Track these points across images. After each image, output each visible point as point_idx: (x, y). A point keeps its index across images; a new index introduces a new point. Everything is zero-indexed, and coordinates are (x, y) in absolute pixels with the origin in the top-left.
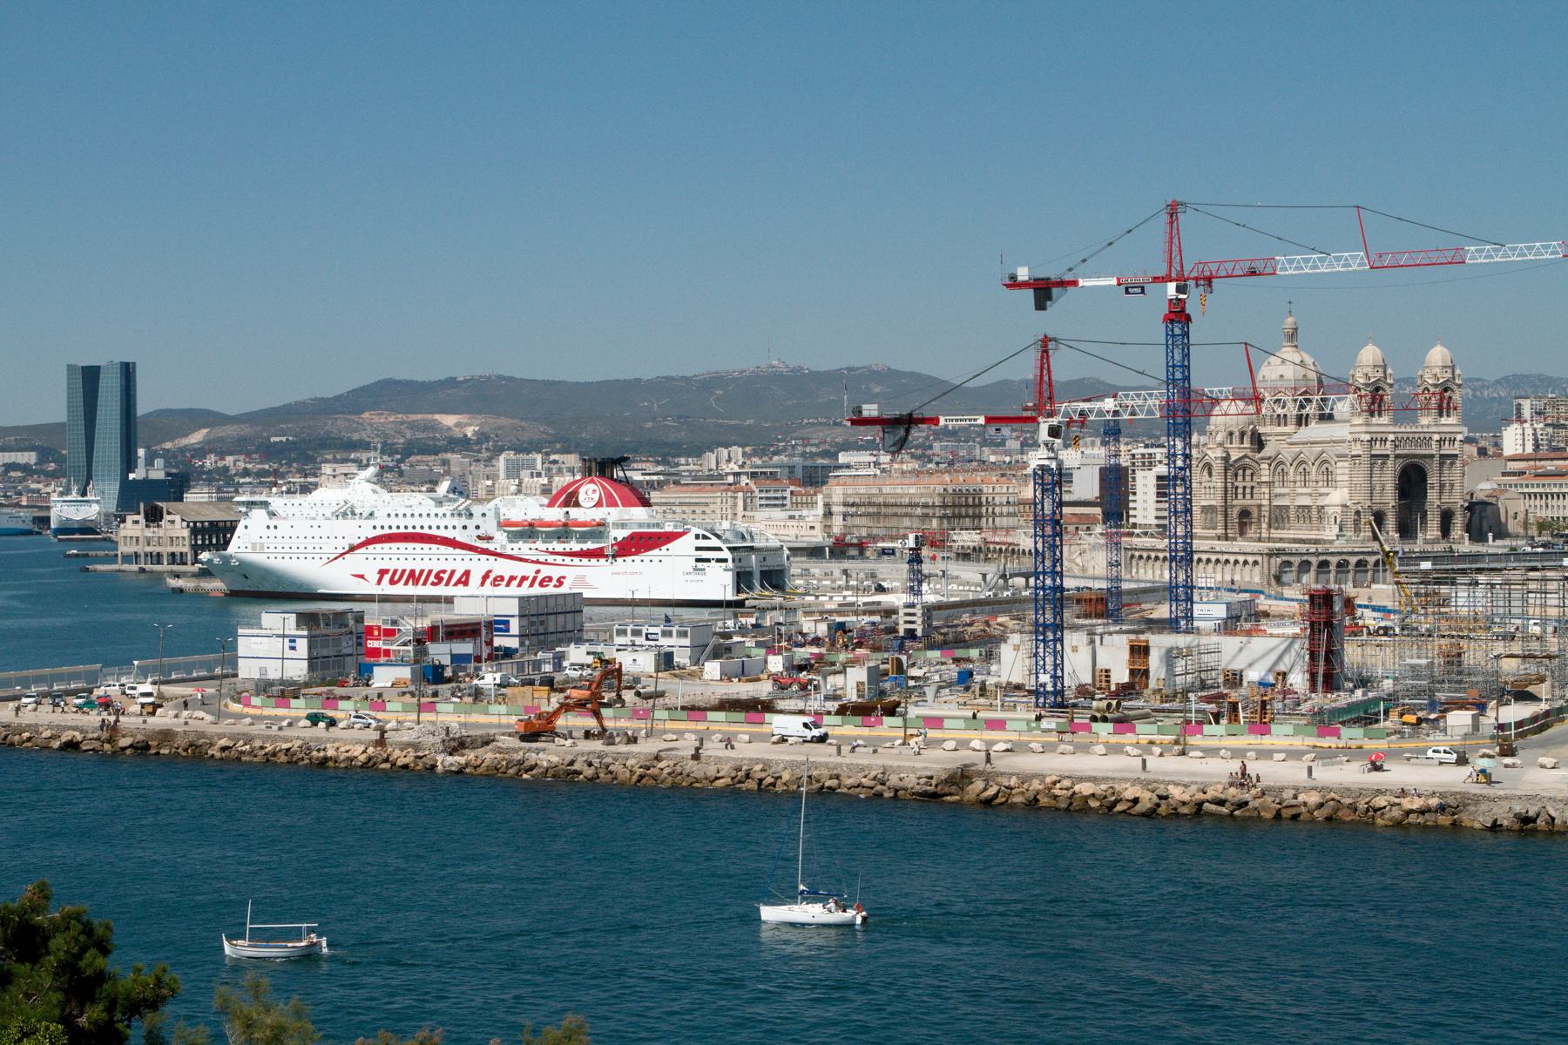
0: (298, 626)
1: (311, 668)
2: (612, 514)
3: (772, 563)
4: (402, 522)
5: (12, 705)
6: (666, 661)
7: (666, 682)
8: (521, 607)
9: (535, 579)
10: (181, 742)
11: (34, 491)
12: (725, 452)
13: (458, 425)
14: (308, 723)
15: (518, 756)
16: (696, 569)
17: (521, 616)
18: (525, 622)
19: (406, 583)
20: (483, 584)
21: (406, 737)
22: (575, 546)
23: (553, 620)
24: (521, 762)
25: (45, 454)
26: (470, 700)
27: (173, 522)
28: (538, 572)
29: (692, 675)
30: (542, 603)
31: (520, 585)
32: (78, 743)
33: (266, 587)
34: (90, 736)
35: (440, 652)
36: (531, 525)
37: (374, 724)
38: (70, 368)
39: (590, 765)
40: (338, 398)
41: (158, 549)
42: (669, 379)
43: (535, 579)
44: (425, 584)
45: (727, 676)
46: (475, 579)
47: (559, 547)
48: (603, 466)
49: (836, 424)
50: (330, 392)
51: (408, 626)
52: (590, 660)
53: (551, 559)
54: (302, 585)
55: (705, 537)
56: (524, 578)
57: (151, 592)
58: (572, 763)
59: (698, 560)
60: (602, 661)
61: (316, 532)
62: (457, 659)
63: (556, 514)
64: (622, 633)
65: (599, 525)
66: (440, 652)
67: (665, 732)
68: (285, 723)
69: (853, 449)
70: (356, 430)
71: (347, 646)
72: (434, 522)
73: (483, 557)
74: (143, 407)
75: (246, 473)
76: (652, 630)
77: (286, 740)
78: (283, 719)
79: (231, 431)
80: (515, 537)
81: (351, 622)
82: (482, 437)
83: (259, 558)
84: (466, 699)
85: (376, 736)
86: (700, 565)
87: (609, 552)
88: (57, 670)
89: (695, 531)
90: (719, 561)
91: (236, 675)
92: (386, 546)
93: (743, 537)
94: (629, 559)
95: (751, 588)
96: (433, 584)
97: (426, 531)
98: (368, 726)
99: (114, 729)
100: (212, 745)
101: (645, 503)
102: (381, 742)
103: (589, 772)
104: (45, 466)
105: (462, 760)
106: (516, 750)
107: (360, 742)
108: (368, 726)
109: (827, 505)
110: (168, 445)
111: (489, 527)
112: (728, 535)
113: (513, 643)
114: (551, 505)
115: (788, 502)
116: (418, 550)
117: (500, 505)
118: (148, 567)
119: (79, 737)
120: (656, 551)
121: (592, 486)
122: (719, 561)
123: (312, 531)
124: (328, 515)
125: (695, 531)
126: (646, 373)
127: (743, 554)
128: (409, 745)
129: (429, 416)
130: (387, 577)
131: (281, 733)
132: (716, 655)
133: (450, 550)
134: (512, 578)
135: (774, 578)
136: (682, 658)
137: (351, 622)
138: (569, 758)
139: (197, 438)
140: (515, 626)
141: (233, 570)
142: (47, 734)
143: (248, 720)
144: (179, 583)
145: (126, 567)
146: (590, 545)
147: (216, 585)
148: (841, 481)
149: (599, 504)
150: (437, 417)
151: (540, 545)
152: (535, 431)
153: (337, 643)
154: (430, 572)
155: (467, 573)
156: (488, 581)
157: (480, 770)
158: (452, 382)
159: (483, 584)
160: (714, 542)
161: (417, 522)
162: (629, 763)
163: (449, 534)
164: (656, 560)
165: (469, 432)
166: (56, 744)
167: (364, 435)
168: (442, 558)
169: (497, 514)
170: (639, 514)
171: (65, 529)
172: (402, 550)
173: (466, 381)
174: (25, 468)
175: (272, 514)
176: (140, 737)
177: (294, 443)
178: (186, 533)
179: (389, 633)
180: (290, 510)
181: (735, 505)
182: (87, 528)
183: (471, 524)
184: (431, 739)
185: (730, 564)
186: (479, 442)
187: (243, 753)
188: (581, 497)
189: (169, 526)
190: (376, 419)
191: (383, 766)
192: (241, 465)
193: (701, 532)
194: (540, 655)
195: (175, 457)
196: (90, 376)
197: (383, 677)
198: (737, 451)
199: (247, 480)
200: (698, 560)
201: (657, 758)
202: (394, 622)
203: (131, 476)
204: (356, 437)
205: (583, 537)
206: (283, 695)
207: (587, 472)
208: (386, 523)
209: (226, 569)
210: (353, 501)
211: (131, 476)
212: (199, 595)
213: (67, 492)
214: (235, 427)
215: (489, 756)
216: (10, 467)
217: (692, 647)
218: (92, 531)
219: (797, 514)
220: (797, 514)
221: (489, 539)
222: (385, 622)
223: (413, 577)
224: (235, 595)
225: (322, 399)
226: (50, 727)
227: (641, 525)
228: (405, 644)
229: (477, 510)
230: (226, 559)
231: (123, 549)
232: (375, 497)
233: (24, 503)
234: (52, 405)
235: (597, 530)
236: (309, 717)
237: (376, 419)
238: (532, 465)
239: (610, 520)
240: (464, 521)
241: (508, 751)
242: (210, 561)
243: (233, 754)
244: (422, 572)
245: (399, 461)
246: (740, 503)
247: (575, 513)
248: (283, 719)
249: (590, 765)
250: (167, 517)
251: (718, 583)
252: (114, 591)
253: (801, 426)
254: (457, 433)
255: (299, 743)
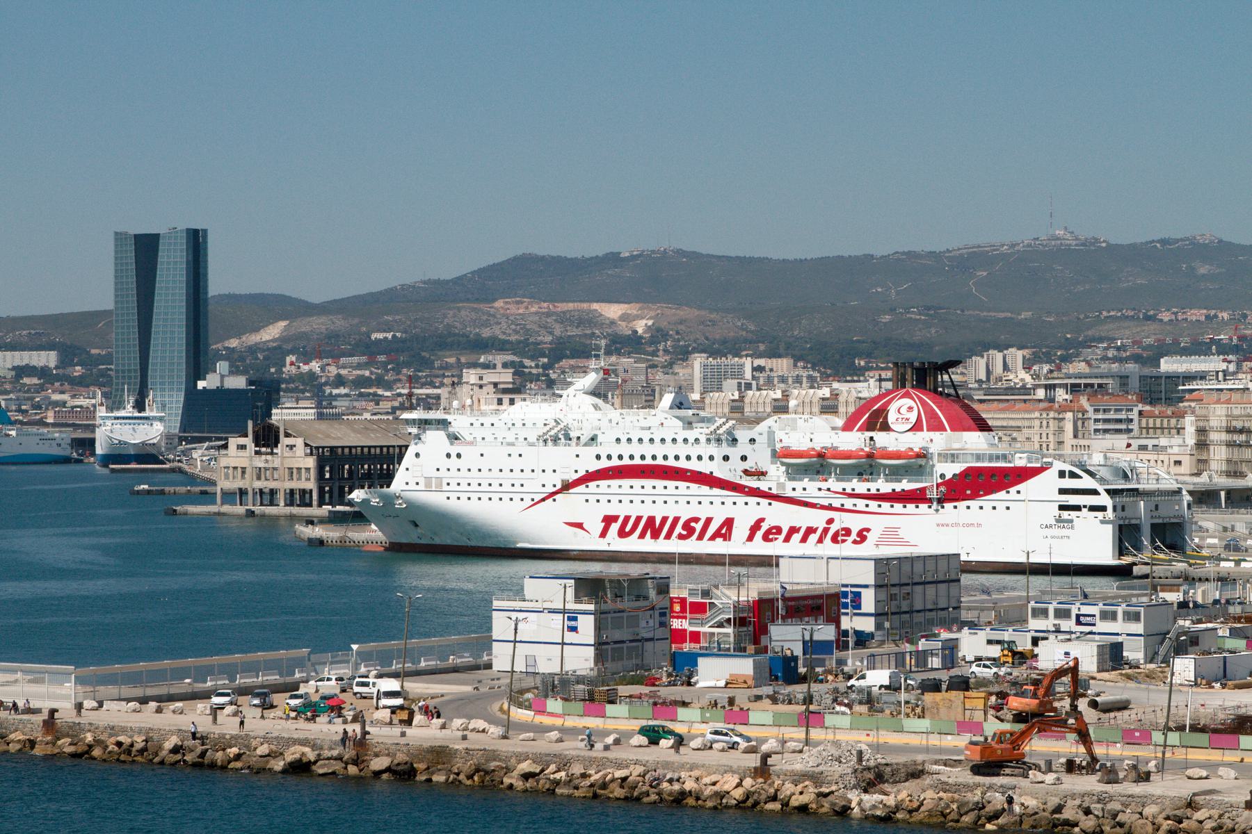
0: (578, 599)
1: (600, 657)
2: (937, 442)
3: (1166, 513)
4: (637, 450)
5: (201, 706)
6: (1113, 656)
7: (1110, 687)
8: (877, 574)
9: (826, 530)
10: (463, 765)
11: (56, 404)
12: (999, 356)
13: (624, 317)
14: (643, 740)
15: (975, 797)
16: (1059, 520)
17: (878, 586)
18: (883, 596)
19: (642, 536)
20: (750, 538)
21: (799, 764)
22: (885, 487)
23: (920, 596)
24: (980, 807)
25: (68, 355)
26: (864, 709)
27: (291, 447)
28: (830, 521)
29: (1150, 676)
30: (906, 568)
31: (804, 540)
32: (309, 763)
33: (464, 542)
34: (327, 753)
35: (787, 637)
36: (821, 455)
37: (743, 745)
38: (119, 237)
39: (1087, 812)
40: (458, 281)
41: (272, 485)
42: (910, 255)
43: (826, 530)
44: (668, 537)
45: (1203, 679)
46: (741, 530)
47: (861, 487)
48: (924, 375)
49: (1148, 318)
50: (448, 272)
51: (727, 598)
52: (995, 651)
53: (849, 503)
54: (497, 536)
55: (1073, 475)
56: (810, 531)
57: (266, 542)
58: (1059, 809)
59: (1062, 508)
60: (1014, 654)
61: (516, 463)
62: (811, 646)
63: (854, 441)
64: (1041, 613)
65: (918, 456)
66: (787, 637)
67: (1187, 765)
68: (610, 740)
69: (1176, 353)
70: (486, 324)
71: (647, 626)
72: (682, 450)
73: (753, 500)
74: (218, 284)
75: (340, 381)
76: (1086, 610)
77: (620, 765)
78: (606, 733)
79: (317, 325)
80: (796, 472)
81: (652, 593)
82: (658, 335)
83: (435, 499)
84: (857, 708)
85: (753, 761)
86: (1065, 515)
87: (934, 495)
88: (251, 657)
89: (1059, 465)
90: (1093, 508)
91: (489, 666)
92: (615, 483)
93: (1125, 476)
94: (962, 505)
95: (1138, 548)
96: (681, 537)
97: (671, 462)
98: (734, 746)
99: (362, 743)
100: (508, 770)
101: (983, 426)
102: (763, 771)
103: (1089, 823)
104: (69, 370)
105: (891, 801)
106: (971, 788)
107: (730, 770)
108: (734, 746)
109: (1201, 431)
110: (233, 343)
111: (760, 458)
112: (1103, 472)
113: (867, 625)
114: (848, 427)
115: (1134, 426)
116: (671, 490)
117: (775, 427)
118: (258, 509)
119: (311, 755)
120: (1001, 495)
121: (907, 402)
122: (1093, 508)
123: (492, 456)
124: (532, 439)
125: (1059, 465)
126: (881, 248)
127: (1125, 499)
128: (805, 776)
129: (585, 306)
130: (615, 527)
131: (610, 755)
132: (1180, 650)
133: (705, 489)
134: (793, 530)
135: (1170, 535)
136: (1134, 652)
137: (652, 593)
138: (1054, 802)
139: (271, 333)
140: (868, 601)
141: (397, 514)
142: (263, 750)
143: (554, 735)
144: (318, 532)
145: (226, 508)
146: (905, 485)
147: (372, 534)
148: (1224, 396)
149: (917, 427)
150: (595, 306)
151: (834, 484)
152: (730, 326)
153: (634, 621)
154: (676, 520)
155: (729, 523)
156: (759, 534)
157: (918, 817)
158: (613, 259)
159: (750, 538)
160: (1086, 482)
161: (659, 450)
162: (1150, 810)
163: (704, 467)
164: (1001, 506)
165: (640, 326)
166: (278, 765)
167: (497, 331)
168: (694, 500)
169: (771, 434)
170: (974, 441)
171: (117, 456)
172: (637, 489)
173: (633, 258)
174: (43, 372)
175: (454, 438)
176: (401, 757)
177: (403, 341)
178: (311, 462)
179: (699, 608)
180: (478, 433)
181: (1061, 430)
182: (146, 455)
183: (735, 453)
184: (837, 769)
185: (1110, 514)
186: (654, 341)
187: (557, 783)
188: (892, 417)
189: (287, 453)
190: (513, 309)
191: (770, 806)
192: (333, 370)
193: (1067, 468)
194: (923, 644)
195: (242, 359)
196: (145, 249)
197: (713, 673)
198: (1017, 356)
199: (343, 391)
200: (1062, 508)
201: (1191, 805)
202: (706, 593)
203: (201, 385)
204: (486, 333)
205: (895, 473)
206: (591, 698)
207: (900, 382)
208: (613, 452)
209: (388, 512)
210: (567, 420)
211: (201, 385)
212: (346, 548)
213: (119, 405)
214: (323, 319)
215: (930, 794)
216: (21, 371)
217: (1147, 635)
218: (152, 458)
219: (1150, 443)
220: (1150, 443)
221: (761, 474)
222: (692, 592)
223: (653, 528)
224: (396, 548)
225: (438, 283)
226: (266, 739)
227: (979, 457)
228: (720, 625)
229: (743, 435)
230: (389, 500)
231: (225, 484)
232: (598, 414)
233: (50, 420)
234: (95, 287)
235: (917, 463)
236: (644, 731)
237: (513, 309)
238: (738, 373)
239: (934, 449)
240: (726, 449)
241: (957, 788)
242: (365, 502)
243: (543, 784)
244: (665, 519)
245: (546, 367)
246: (1069, 427)
247: (883, 440)
248: (606, 733)
249: (1087, 812)
250: (285, 441)
251: (1093, 542)
252: (211, 544)
253: (1099, 321)
254: (624, 329)
255: (640, 769)
